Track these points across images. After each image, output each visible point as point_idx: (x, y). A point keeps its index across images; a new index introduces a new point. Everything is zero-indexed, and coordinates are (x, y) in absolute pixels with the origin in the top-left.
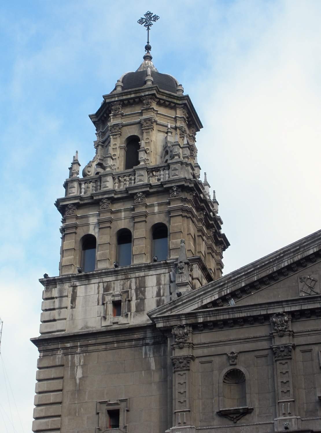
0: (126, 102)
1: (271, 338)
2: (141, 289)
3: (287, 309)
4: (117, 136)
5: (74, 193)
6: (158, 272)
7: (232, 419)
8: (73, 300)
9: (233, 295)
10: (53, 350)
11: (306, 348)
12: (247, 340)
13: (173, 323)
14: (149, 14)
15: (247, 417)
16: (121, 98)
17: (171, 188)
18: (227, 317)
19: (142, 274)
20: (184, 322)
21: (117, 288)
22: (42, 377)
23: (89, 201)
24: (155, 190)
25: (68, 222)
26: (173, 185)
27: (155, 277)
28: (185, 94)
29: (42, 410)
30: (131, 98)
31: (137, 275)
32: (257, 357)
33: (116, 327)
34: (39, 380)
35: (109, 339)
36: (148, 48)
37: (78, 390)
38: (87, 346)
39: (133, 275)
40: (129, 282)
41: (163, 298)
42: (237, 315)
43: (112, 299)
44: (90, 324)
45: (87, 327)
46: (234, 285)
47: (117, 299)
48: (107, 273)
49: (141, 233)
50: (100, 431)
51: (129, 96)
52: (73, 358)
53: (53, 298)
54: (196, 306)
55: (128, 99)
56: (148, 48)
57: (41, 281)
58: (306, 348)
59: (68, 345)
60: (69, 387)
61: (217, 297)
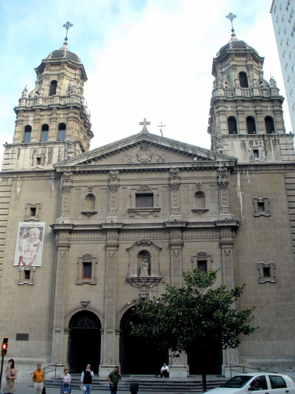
0: (53, 64)
1: (109, 181)
2: (51, 153)
6: (60, 146)
7: (88, 216)
8: (18, 155)
10: (7, 178)
14: (68, 23)
16: (51, 62)
17: (70, 107)
19: (52, 146)
20: (69, 170)
26: (71, 105)
28: (81, 63)
30: (55, 62)
31: (50, 146)
35: (34, 175)
37: (18, 198)
38: (23, 177)
39: (48, 146)
42: (95, 169)
43: (37, 156)
47: (39, 157)
48: (36, 144)
49: (53, 127)
51: (55, 61)
53: (9, 154)
54: (76, 163)
59: (14, 176)
60: (13, 196)
61: (86, 160)
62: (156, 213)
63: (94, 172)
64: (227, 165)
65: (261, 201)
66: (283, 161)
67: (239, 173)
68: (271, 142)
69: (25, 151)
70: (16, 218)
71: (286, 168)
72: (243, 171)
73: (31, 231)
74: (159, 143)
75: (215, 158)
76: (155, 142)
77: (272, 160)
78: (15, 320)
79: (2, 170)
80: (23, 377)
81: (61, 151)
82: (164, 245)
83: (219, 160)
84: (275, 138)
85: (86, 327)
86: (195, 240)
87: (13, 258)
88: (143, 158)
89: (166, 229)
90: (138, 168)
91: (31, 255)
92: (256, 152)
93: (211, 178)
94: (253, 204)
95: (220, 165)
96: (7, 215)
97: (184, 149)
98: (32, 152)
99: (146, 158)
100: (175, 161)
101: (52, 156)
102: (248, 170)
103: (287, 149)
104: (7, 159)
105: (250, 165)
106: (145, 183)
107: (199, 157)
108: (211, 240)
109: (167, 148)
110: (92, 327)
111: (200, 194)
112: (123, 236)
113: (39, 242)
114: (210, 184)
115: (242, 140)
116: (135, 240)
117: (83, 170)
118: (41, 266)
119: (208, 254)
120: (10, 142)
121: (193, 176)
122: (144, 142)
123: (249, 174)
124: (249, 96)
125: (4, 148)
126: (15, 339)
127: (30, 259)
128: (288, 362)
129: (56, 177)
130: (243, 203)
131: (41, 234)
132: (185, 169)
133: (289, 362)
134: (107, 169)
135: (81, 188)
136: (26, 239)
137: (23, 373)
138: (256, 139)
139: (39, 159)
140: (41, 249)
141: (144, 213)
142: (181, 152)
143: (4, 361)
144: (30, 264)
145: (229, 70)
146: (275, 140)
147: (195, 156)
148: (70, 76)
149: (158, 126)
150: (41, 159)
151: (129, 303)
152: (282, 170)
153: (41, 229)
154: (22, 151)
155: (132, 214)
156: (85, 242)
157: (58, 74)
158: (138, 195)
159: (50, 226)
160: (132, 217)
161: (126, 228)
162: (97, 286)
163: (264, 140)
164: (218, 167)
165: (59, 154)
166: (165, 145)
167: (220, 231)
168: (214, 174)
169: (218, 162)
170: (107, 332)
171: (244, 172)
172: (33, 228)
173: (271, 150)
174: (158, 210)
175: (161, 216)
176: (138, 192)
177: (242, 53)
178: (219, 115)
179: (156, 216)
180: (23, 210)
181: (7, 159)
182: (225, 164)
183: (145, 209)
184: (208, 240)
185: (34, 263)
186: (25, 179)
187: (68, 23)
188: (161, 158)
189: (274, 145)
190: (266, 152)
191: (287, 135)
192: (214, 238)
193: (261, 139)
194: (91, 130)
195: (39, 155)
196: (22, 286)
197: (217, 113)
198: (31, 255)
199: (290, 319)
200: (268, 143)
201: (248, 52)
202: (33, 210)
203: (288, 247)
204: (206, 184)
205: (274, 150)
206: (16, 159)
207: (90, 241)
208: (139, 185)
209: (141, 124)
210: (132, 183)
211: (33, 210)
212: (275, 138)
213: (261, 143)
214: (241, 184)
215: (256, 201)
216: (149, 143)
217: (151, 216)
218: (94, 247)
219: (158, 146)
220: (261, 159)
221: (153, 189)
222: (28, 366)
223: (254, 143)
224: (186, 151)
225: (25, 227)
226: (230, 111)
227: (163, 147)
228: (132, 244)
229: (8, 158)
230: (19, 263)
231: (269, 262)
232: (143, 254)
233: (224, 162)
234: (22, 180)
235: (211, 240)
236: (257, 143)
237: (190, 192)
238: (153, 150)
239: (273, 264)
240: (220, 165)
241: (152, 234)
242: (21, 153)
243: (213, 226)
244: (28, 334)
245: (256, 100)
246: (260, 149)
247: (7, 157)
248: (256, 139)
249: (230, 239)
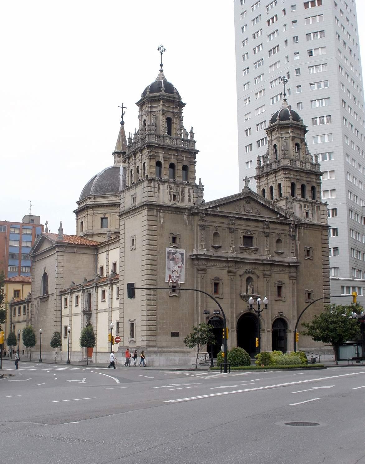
0: (168, 100)
1: (229, 224)
2: (183, 192)
4: (165, 116)
5: (324, 197)
6: (189, 187)
7: (215, 249)
8: (159, 190)
9: (218, 206)
10: (152, 209)
11: (224, 228)
12: (253, 226)
13: (200, 211)
15: (219, 249)
16: (167, 98)
17: (192, 152)
18: (217, 214)
19: (184, 186)
20: (204, 212)
21: (174, 190)
23: (161, 147)
24: (186, 151)
26: (193, 151)
27: (188, 189)
29: (150, 232)
30: (171, 100)
31: (182, 186)
32: (223, 229)
33: (175, 205)
35: (173, 209)
36: (161, 65)
37: (162, 227)
38: (165, 210)
39: (180, 186)
40: (179, 188)
41: (190, 198)
42: (220, 214)
43: (173, 193)
45: (165, 203)
46: (219, 203)
47: (175, 194)
49: (179, 167)
51: (170, 99)
52: (160, 214)
53: (151, 187)
56: (161, 65)
58: (224, 228)
59: (158, 208)
60: (159, 225)
62: (256, 251)
63: (219, 216)
64: (296, 223)
65: (308, 249)
66: (321, 222)
67: (298, 228)
68: (316, 207)
69: (163, 186)
70: (163, 244)
71: (323, 228)
72: (300, 226)
73: (175, 255)
74: (258, 200)
75: (290, 217)
76: (256, 199)
77: (315, 222)
80: (180, 361)
81: (190, 192)
82: (261, 274)
83: (292, 219)
84: (318, 205)
87: (164, 276)
88: (247, 209)
89: (263, 264)
91: (177, 274)
92: (307, 213)
93: (285, 230)
94: (305, 250)
95: (292, 223)
96: (156, 240)
97: (272, 207)
98: (169, 189)
99: (249, 209)
101: (184, 195)
102: (303, 227)
103: (324, 215)
104: (150, 192)
105: (305, 224)
106: (249, 228)
108: (285, 273)
109: (262, 204)
111: (279, 241)
112: (238, 266)
113: (181, 265)
114: (285, 235)
115: (300, 204)
117: (213, 213)
118: (184, 283)
119: (283, 282)
121: (276, 228)
122: (249, 197)
123: (303, 229)
126: (171, 336)
127: (176, 277)
128: (317, 349)
129: (189, 214)
130: (299, 250)
131: (183, 259)
132: (273, 222)
133: (317, 350)
134: (228, 215)
135: (210, 226)
136: (173, 262)
137: (180, 359)
138: (308, 204)
139: (174, 196)
140: (184, 270)
142: (270, 209)
144: (177, 281)
145: (289, 138)
146: (318, 206)
149: (123, 103)
150: (120, 168)
151: (242, 312)
152: (320, 229)
153: (182, 254)
154: (161, 186)
155: (242, 250)
156: (215, 268)
157: (173, 112)
158: (245, 237)
160: (242, 252)
161: (242, 261)
162: (223, 300)
163: (312, 205)
165: (189, 194)
166: (261, 202)
168: (287, 228)
170: (231, 331)
171: (301, 228)
172: (177, 253)
173: (315, 214)
174: (257, 250)
175: (258, 254)
176: (245, 235)
177: (299, 128)
178: (286, 180)
179: (256, 254)
180: (167, 239)
181: (150, 192)
182: (295, 222)
183: (250, 248)
184: (283, 273)
185: (179, 280)
186: (166, 211)
188: (258, 211)
189: (317, 210)
190: (312, 215)
193: (311, 204)
195: (175, 193)
196: (172, 298)
198: (177, 274)
200: (314, 208)
201: (303, 128)
202: (174, 239)
204: (283, 234)
205: (317, 214)
206: (157, 193)
207: (218, 267)
208: (245, 229)
210: (242, 227)
211: (174, 239)
212: (318, 205)
213: (310, 208)
214: (298, 236)
215: (306, 249)
216: (252, 198)
217: (252, 254)
218: (221, 273)
219: (257, 202)
220: (309, 220)
221: (253, 234)
222: (182, 354)
223: (307, 207)
224: (274, 209)
225: (171, 252)
226: (292, 178)
229: (151, 191)
230: (169, 280)
231: (311, 290)
232: (249, 280)
233: (294, 221)
234: (164, 212)
235: (285, 273)
236: (308, 208)
237: (274, 239)
239: (312, 291)
241: (254, 266)
242: (160, 188)
243: (288, 264)
244: (179, 332)
245: (308, 172)
246: (310, 212)
247: (149, 189)
248: (308, 204)
249: (295, 274)
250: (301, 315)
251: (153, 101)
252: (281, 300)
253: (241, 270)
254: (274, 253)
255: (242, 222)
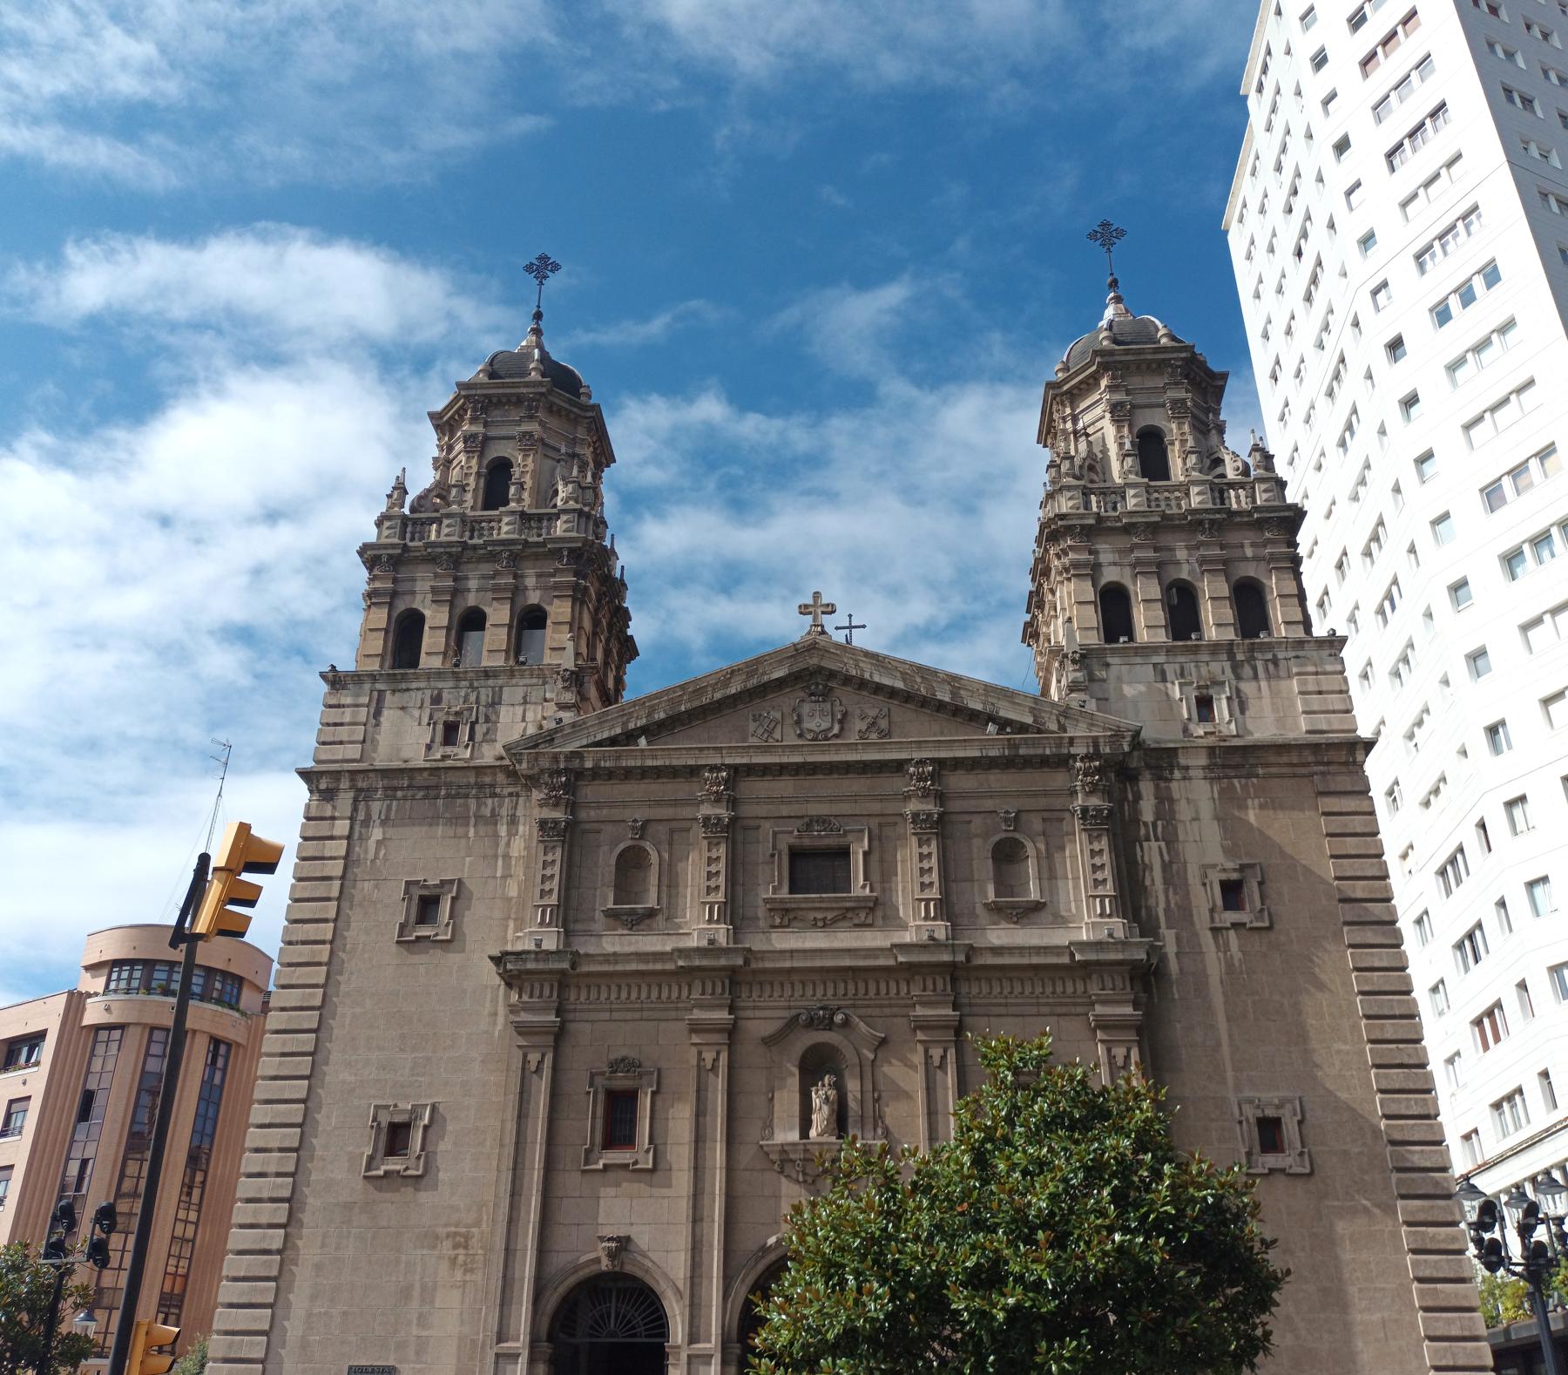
3: (728, 761)
9: (644, 731)
12: (855, 798)
14: (543, 259)
22: (309, 834)
25: (378, 585)
28: (592, 402)
29: (304, 888)
34: (305, 839)
44: (406, 753)
48: (439, 674)
50: (396, 911)
54: (578, 744)
55: (498, 395)
57: (323, 676)
61: (619, 731)
74: (867, 676)
78: (345, 1314)
79: (317, 762)
85: (613, 1334)
86: (1002, 1010)
90: (797, 759)
95: (1079, 750)
99: (825, 725)
100: (920, 741)
103: (1320, 693)
104: (336, 725)
107: (1003, 724)
108: (1059, 1010)
109: (892, 693)
110: (634, 1335)
114: (1046, 815)
116: (789, 1008)
120: (347, 664)
124: (1175, 511)
125: (324, 687)
134: (691, 762)
141: (820, 915)
142: (941, 706)
143: (797, 1120)
147: (992, 718)
148: (557, 445)
158: (796, 854)
159: (492, 958)
164: (1074, 757)
166: (886, 681)
167: (1086, 978)
169: (1071, 740)
181: (336, 725)
187: (543, 259)
191: (1320, 642)
192: (1066, 1004)
194: (629, 632)
197: (1060, 574)
199: (1376, 1317)
202: (426, 906)
203: (1345, 1042)
204: (1032, 815)
209: (804, 610)
211: (426, 906)
227: (878, 689)
228: (778, 1024)
235: (1059, 1010)
238: (846, 698)
240: (1079, 750)
243: (1066, 960)
250: (281, 1150)
251: (1144, 366)
252: (1283, 1171)
253: (768, 1013)
254: (979, 909)
255: (785, 786)
